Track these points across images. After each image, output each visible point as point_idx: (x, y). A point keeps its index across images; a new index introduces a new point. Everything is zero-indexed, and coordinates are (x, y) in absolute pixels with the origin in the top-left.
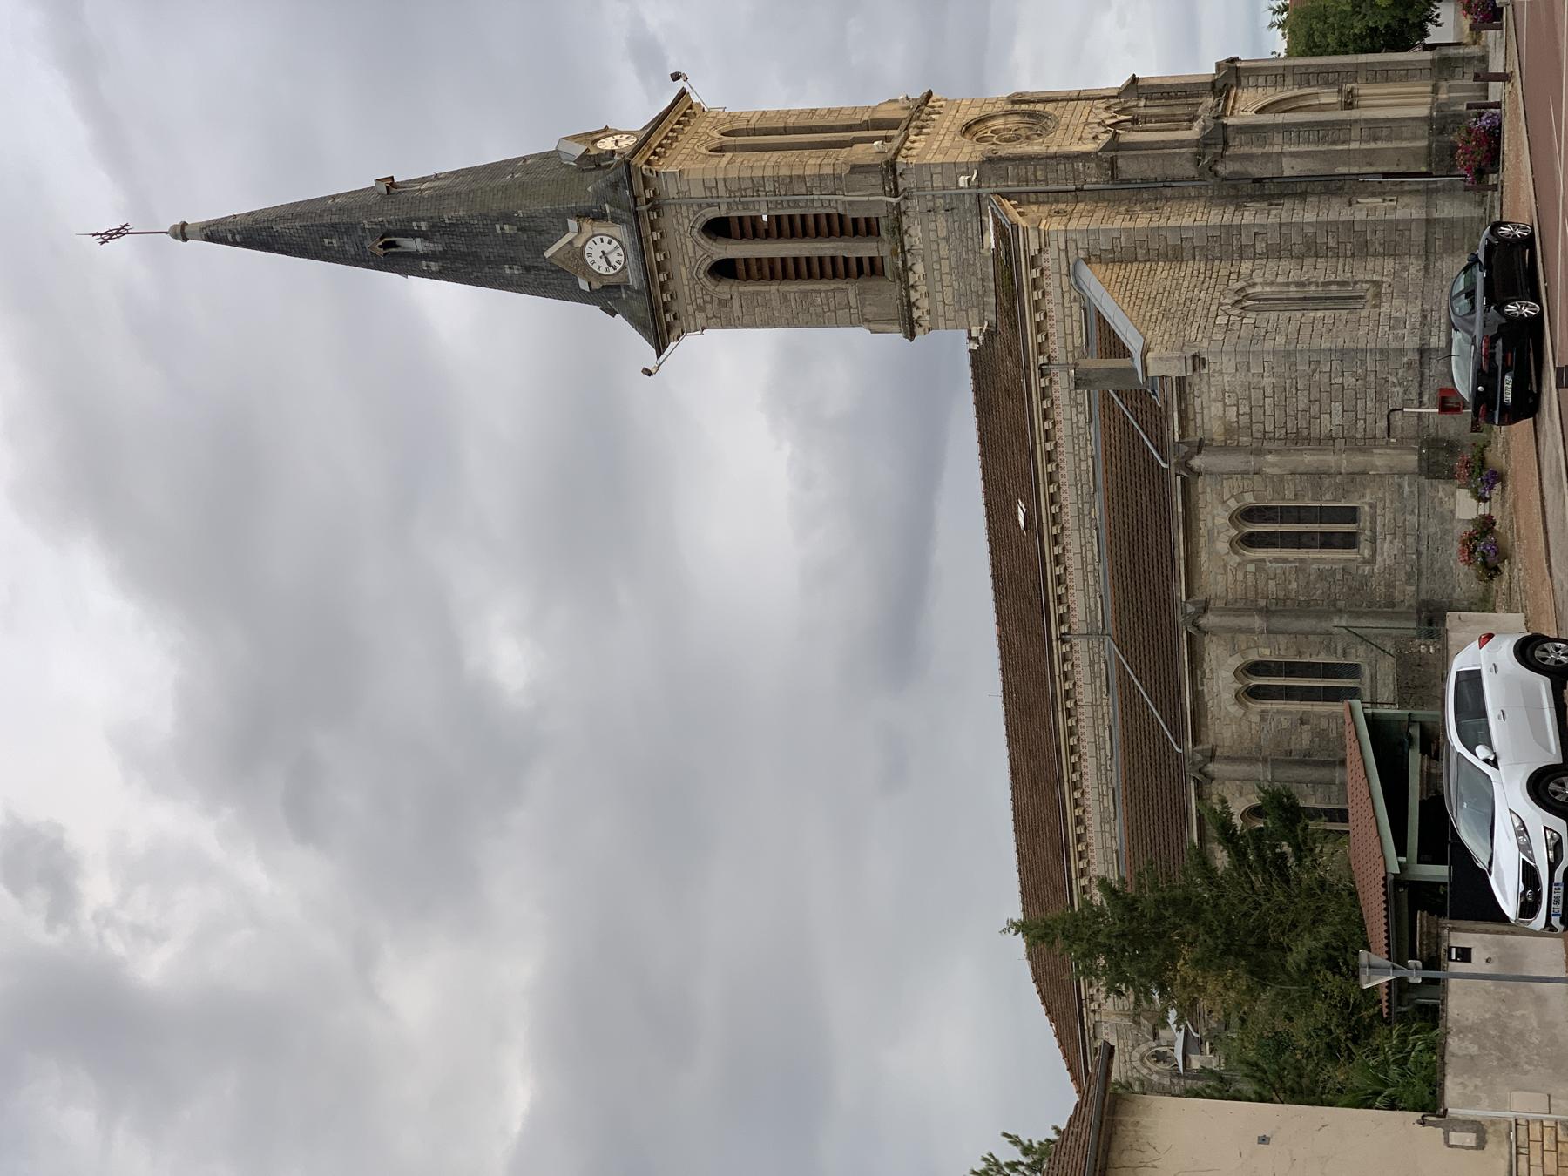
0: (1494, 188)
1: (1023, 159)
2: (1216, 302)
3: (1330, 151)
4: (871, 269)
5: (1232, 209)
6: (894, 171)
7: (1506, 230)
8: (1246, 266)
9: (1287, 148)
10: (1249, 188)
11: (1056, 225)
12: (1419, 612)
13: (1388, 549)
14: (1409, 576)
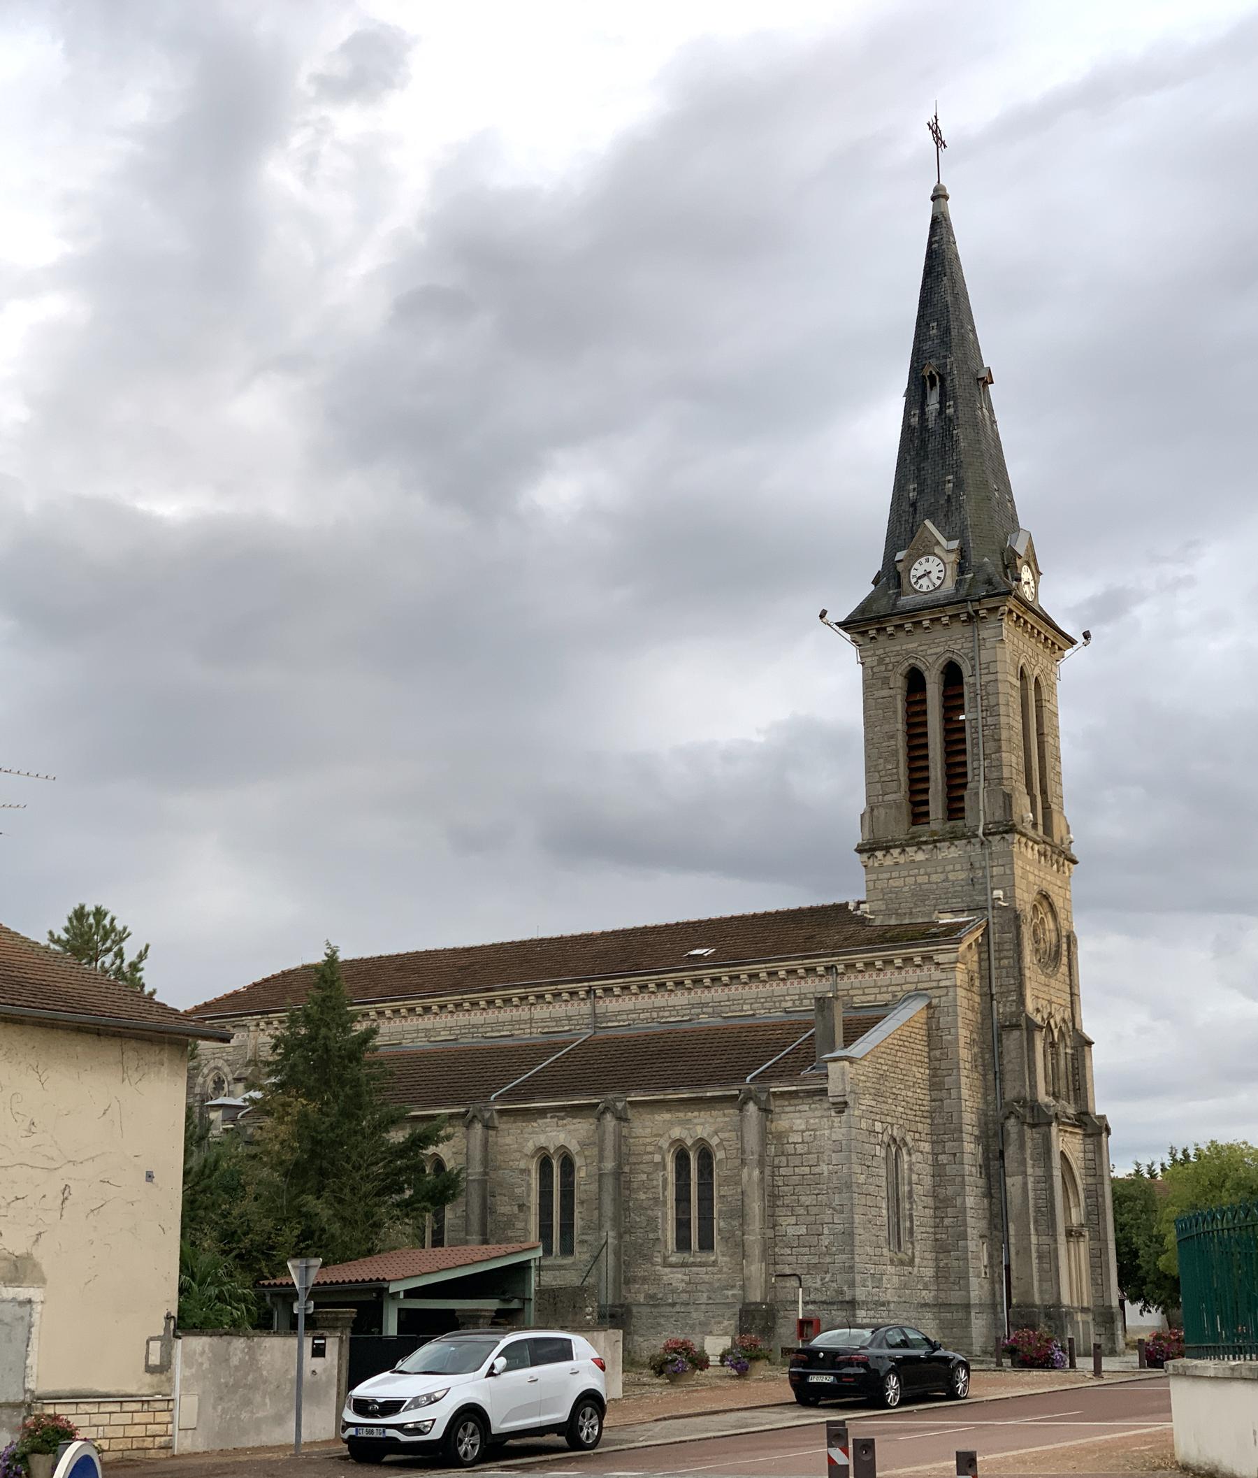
0: (999, 1364)
1: (1018, 948)
4: (918, 815)
5: (977, 1133)
6: (1006, 832)
8: (926, 1147)
9: (1030, 1179)
10: (995, 1147)
11: (960, 977)
12: (622, 1306)
13: (676, 1278)
14: (653, 1297)
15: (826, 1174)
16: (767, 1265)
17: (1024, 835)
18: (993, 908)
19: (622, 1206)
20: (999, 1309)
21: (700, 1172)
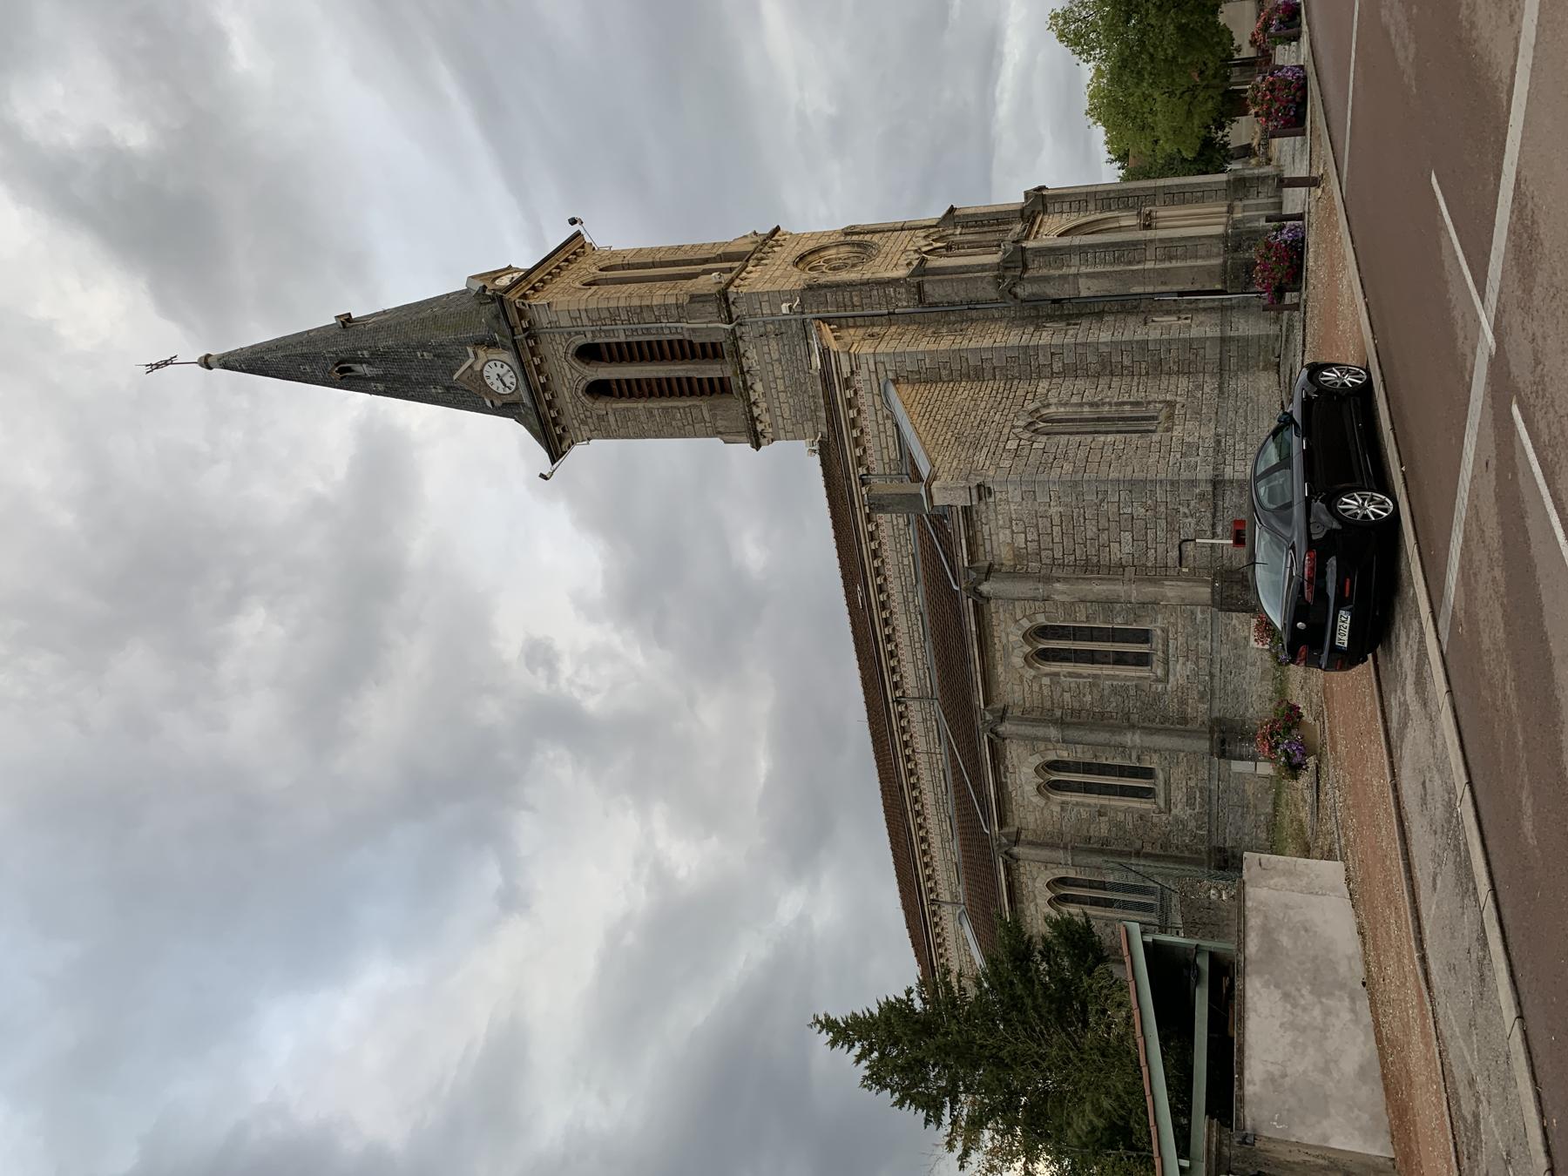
1: (840, 286)
4: (720, 388)
6: (727, 300)
8: (1044, 384)
9: (1083, 270)
10: (1049, 309)
11: (866, 349)
12: (1211, 731)
13: (1181, 671)
16: (1167, 577)
17: (732, 281)
19: (1099, 720)
21: (1067, 638)
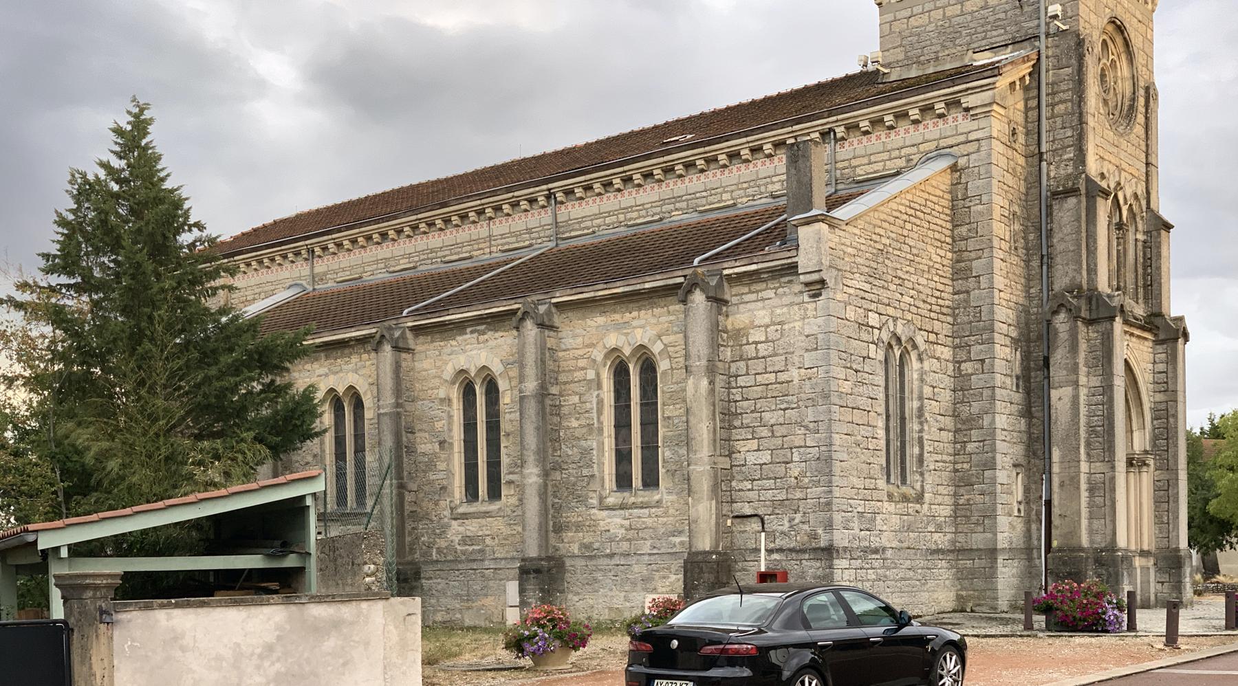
0: (1029, 626)
2: (899, 314)
3: (1078, 440)
5: (1014, 334)
7: (951, 664)
8: (946, 353)
9: (1083, 392)
10: (1038, 354)
11: (997, 126)
12: (549, 559)
13: (614, 523)
14: (587, 547)
15: (796, 381)
18: (1048, 35)
20: (1035, 555)
